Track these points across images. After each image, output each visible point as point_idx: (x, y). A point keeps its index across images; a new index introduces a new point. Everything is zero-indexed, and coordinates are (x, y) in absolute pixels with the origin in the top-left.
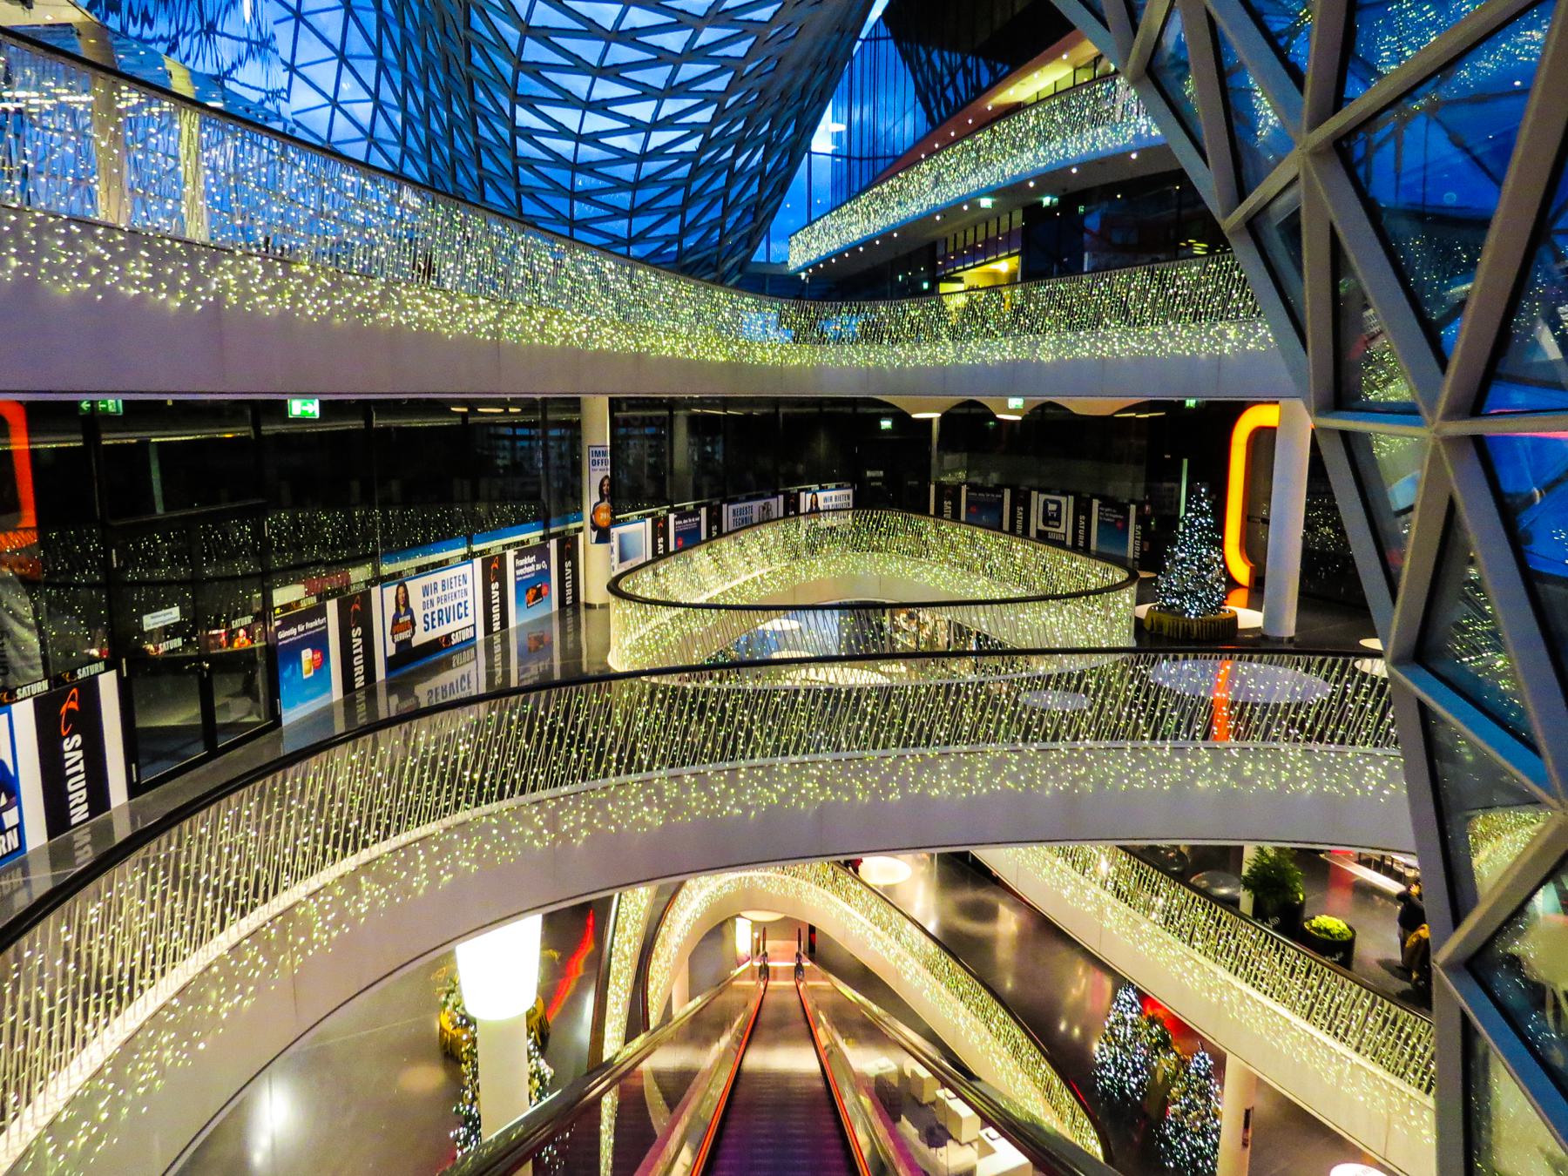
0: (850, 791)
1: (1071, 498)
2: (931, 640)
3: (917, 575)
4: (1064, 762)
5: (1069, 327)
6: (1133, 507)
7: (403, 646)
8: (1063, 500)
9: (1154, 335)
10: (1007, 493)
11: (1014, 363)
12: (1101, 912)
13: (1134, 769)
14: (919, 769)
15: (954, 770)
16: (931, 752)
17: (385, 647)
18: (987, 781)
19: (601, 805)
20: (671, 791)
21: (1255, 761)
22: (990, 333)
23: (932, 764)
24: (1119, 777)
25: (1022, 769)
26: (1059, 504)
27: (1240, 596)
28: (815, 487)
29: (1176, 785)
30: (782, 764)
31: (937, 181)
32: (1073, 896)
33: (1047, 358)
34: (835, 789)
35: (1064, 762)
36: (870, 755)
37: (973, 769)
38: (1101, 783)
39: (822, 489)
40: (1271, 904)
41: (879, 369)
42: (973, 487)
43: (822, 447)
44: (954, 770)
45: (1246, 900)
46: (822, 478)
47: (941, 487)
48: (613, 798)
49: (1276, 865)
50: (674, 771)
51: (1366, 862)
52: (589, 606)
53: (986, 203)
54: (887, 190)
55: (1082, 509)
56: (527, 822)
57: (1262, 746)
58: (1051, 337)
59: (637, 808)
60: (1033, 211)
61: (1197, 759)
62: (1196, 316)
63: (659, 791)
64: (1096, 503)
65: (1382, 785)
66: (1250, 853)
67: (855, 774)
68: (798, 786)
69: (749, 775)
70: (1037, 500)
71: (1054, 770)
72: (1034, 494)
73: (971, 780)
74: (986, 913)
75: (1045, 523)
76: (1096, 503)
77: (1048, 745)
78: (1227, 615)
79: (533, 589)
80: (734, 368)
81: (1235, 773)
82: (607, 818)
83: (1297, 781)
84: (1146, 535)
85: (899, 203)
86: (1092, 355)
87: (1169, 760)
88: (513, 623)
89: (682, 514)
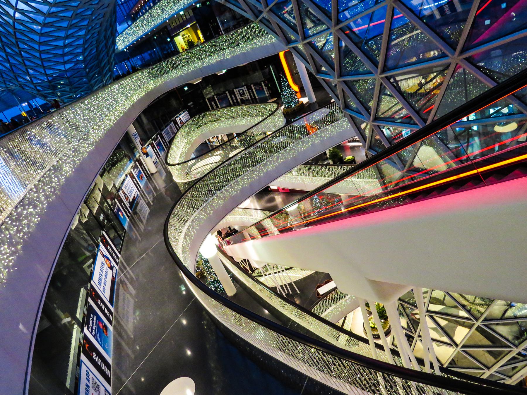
0: (254, 178)
1: (245, 87)
2: (223, 140)
3: (220, 126)
4: (290, 151)
5: (231, 47)
6: (262, 83)
7: (129, 202)
8: (243, 88)
9: (255, 43)
10: (227, 92)
11: (221, 61)
12: (303, 181)
13: (303, 145)
14: (264, 166)
15: (271, 163)
16: (265, 162)
17: (128, 205)
18: (277, 162)
19: (211, 205)
20: (222, 195)
21: (324, 132)
22: (209, 55)
23: (265, 165)
24: (301, 148)
25: (283, 157)
26: (242, 90)
27: (299, 95)
28: (178, 115)
29: (312, 145)
30: (239, 179)
31: (163, 11)
32: (295, 181)
33: (229, 57)
34: (251, 178)
35: (290, 151)
36: (254, 169)
37: (274, 161)
38: (298, 151)
39: (180, 115)
40: (336, 160)
41: (181, 76)
42: (217, 95)
43: (174, 103)
44: (271, 163)
45: (331, 162)
46: (178, 112)
47: (209, 99)
48: (213, 202)
49: (334, 151)
50: (221, 191)
51: (350, 142)
52: (152, 174)
53: (182, 13)
54: (146, 17)
55: (249, 89)
56: (202, 215)
57: (323, 129)
58: (227, 51)
59: (218, 202)
60: (194, 9)
61: (313, 137)
62: (263, 35)
63: (220, 196)
64: (252, 86)
65: (347, 125)
66: (327, 152)
67: (253, 174)
68: (244, 182)
69: (234, 185)
70: (236, 91)
71: (289, 153)
72: (235, 90)
73: (274, 163)
74: (273, 200)
75: (241, 96)
76: (252, 86)
77: (285, 149)
78: (300, 103)
79: (140, 176)
80: (148, 94)
81: (321, 137)
82: (214, 207)
83: (332, 132)
84: (269, 89)
85: (153, 20)
86: (241, 53)
87: (308, 140)
88: (142, 187)
89: (155, 140)
